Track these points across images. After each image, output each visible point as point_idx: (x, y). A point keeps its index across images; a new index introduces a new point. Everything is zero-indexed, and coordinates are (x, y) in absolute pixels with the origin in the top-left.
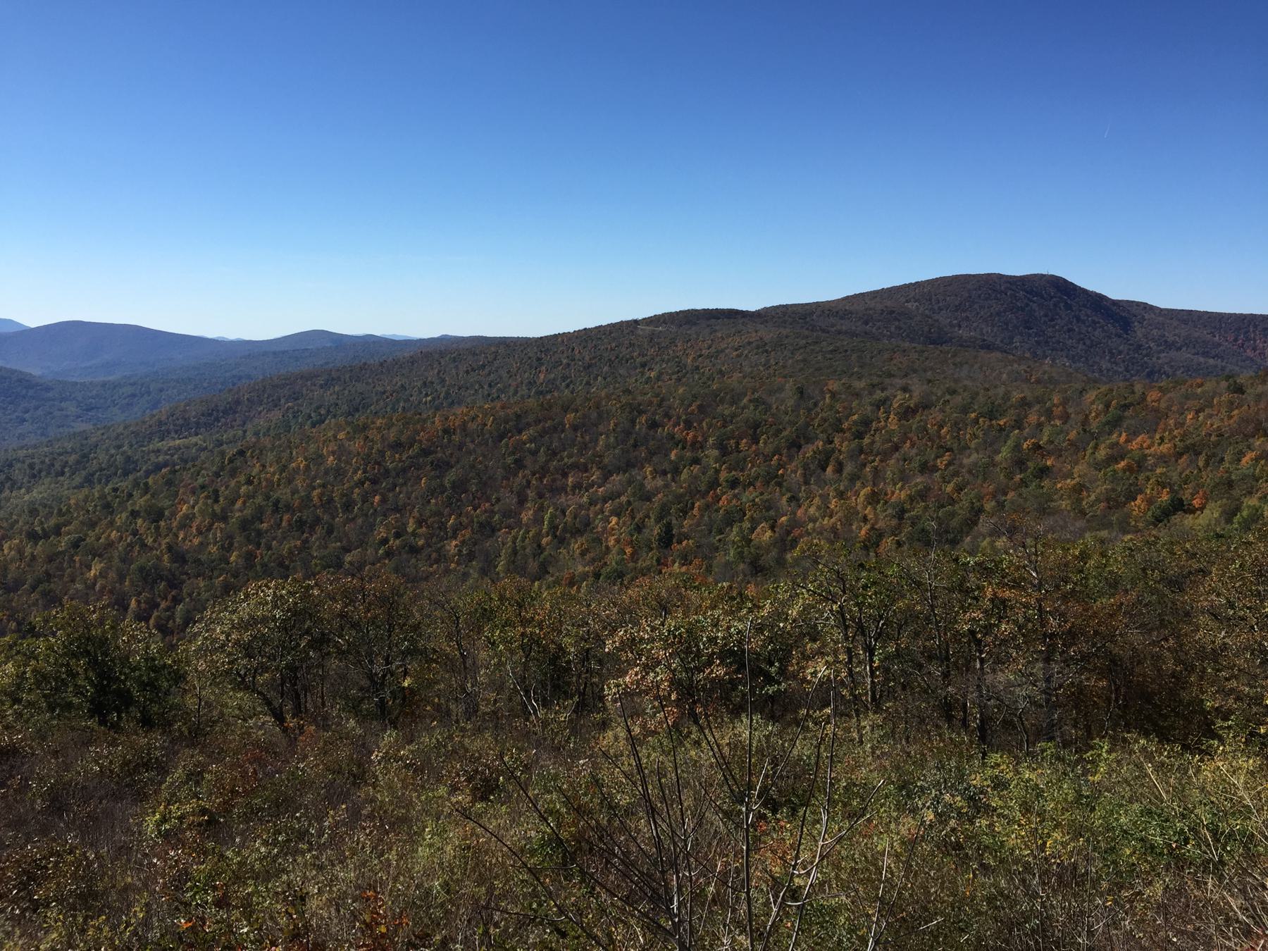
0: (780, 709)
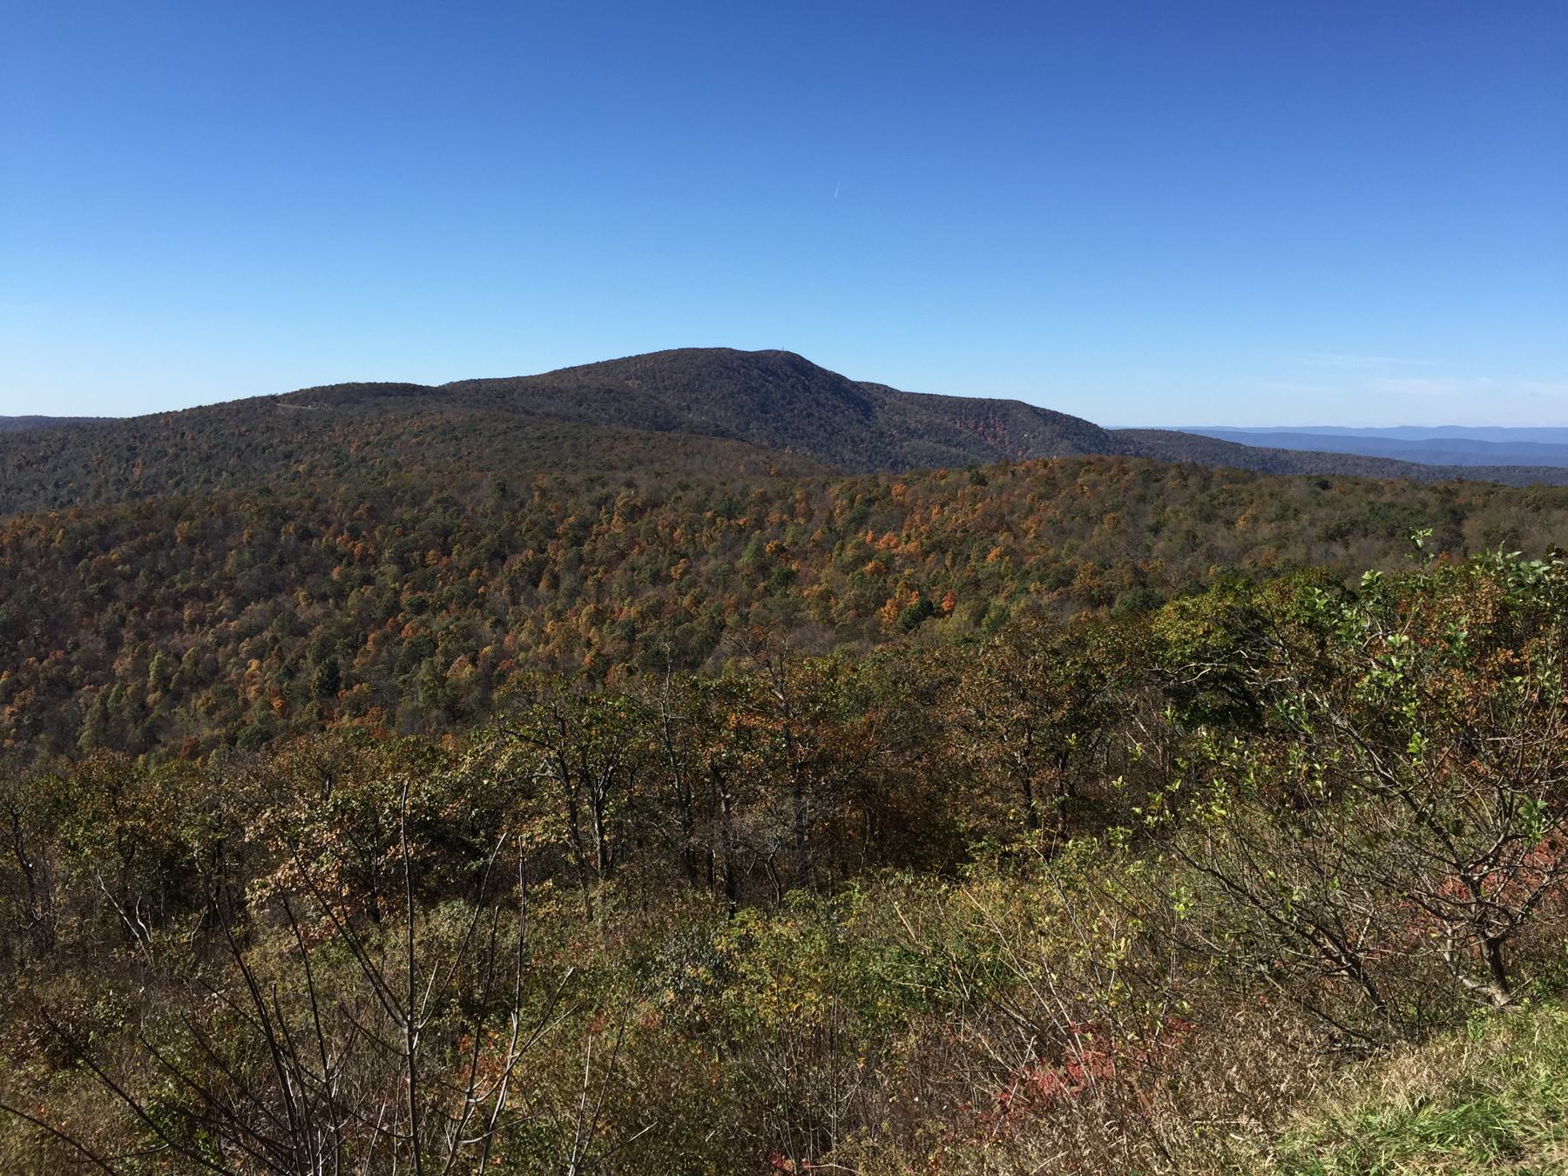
0: (488, 889)
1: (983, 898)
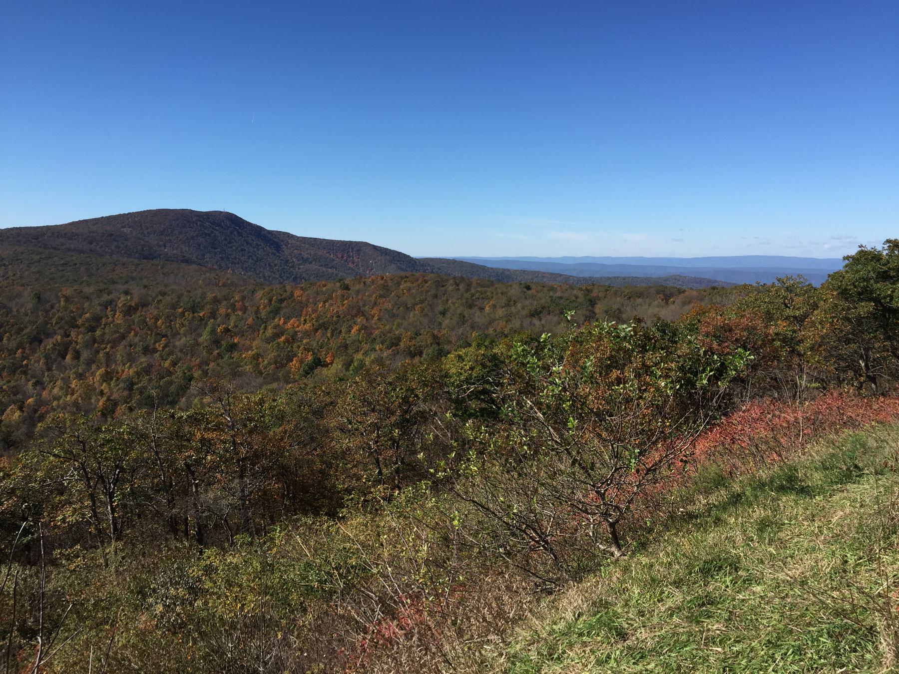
1: (352, 528)
